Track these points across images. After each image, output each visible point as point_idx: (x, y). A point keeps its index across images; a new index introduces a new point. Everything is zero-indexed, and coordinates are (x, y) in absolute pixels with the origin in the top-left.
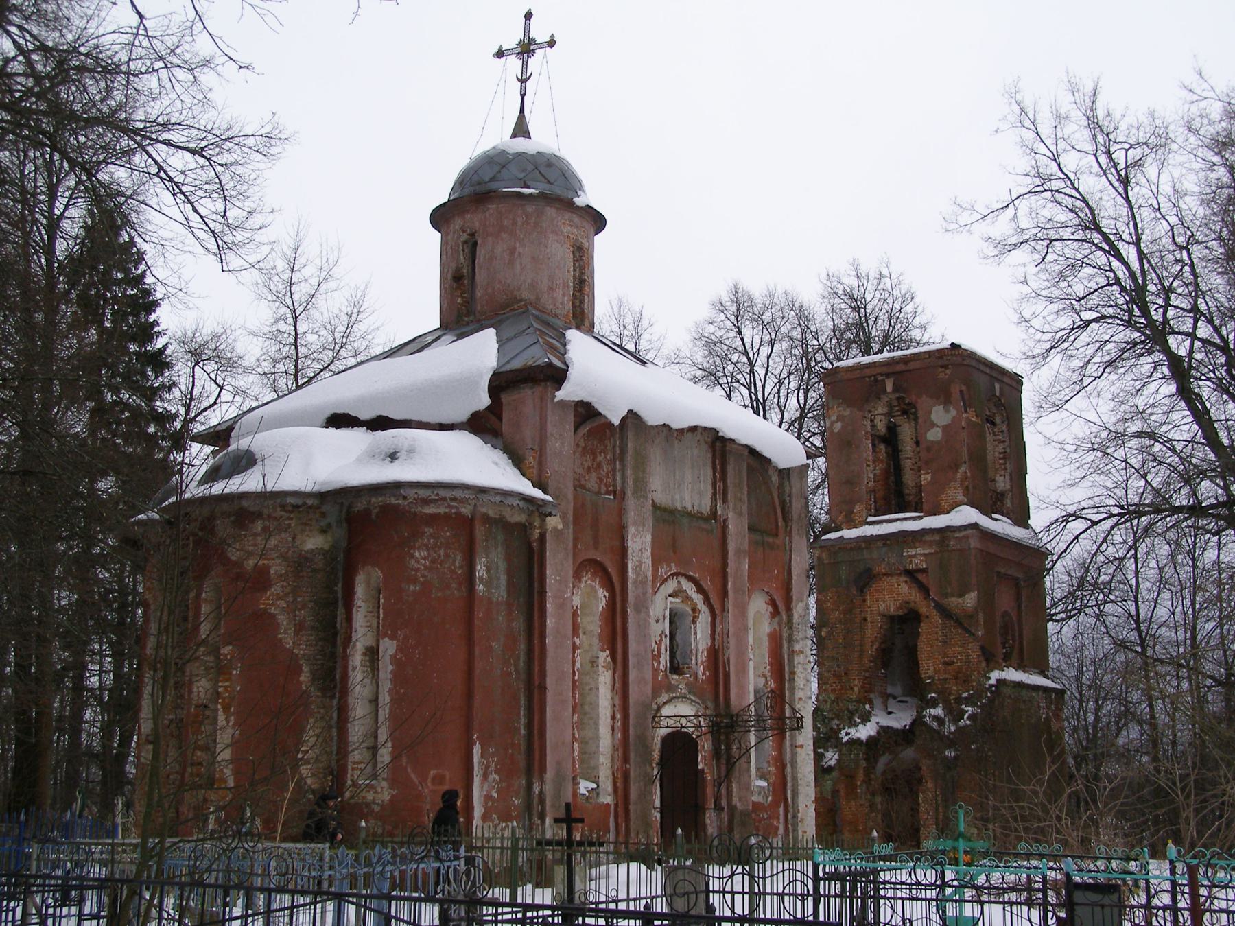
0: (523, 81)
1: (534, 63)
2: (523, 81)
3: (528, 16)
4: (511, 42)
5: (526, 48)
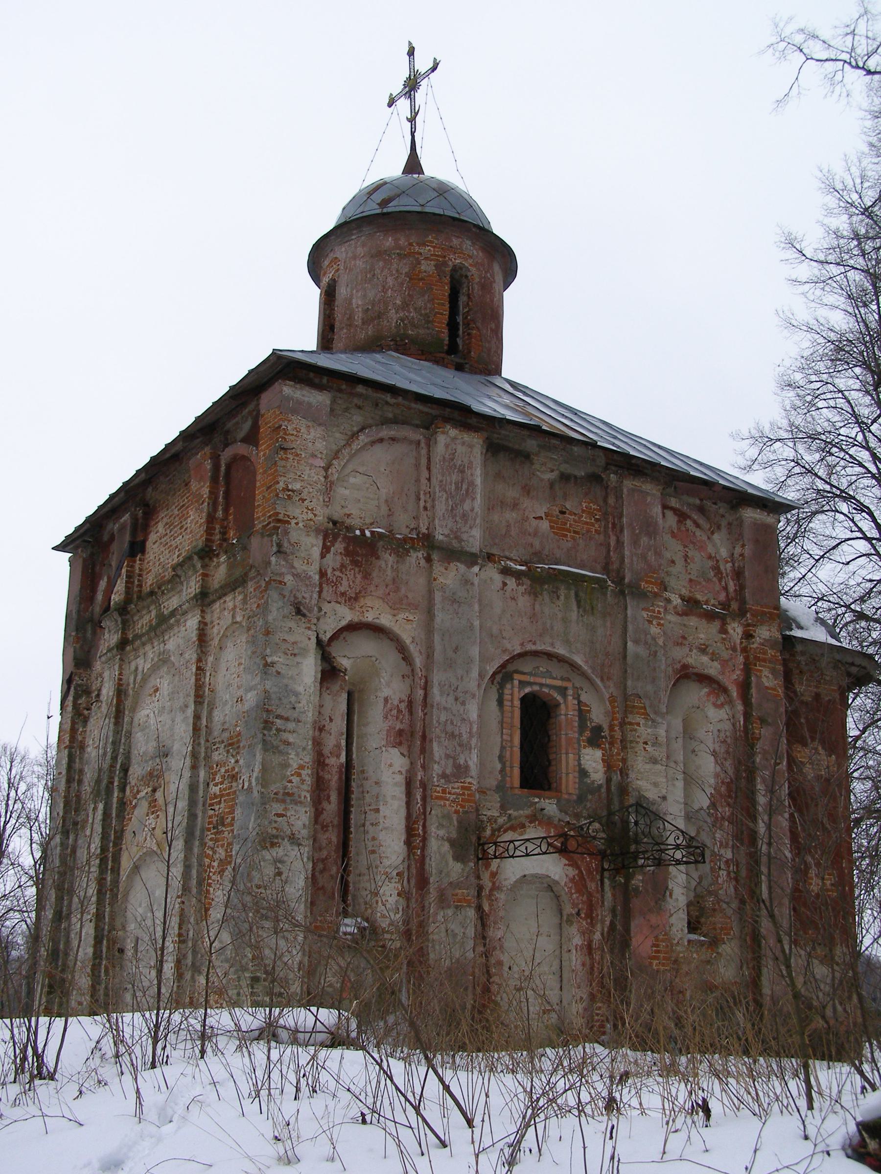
0: (412, 120)
1: (420, 95)
2: (412, 120)
3: (411, 52)
4: (397, 87)
5: (412, 85)
